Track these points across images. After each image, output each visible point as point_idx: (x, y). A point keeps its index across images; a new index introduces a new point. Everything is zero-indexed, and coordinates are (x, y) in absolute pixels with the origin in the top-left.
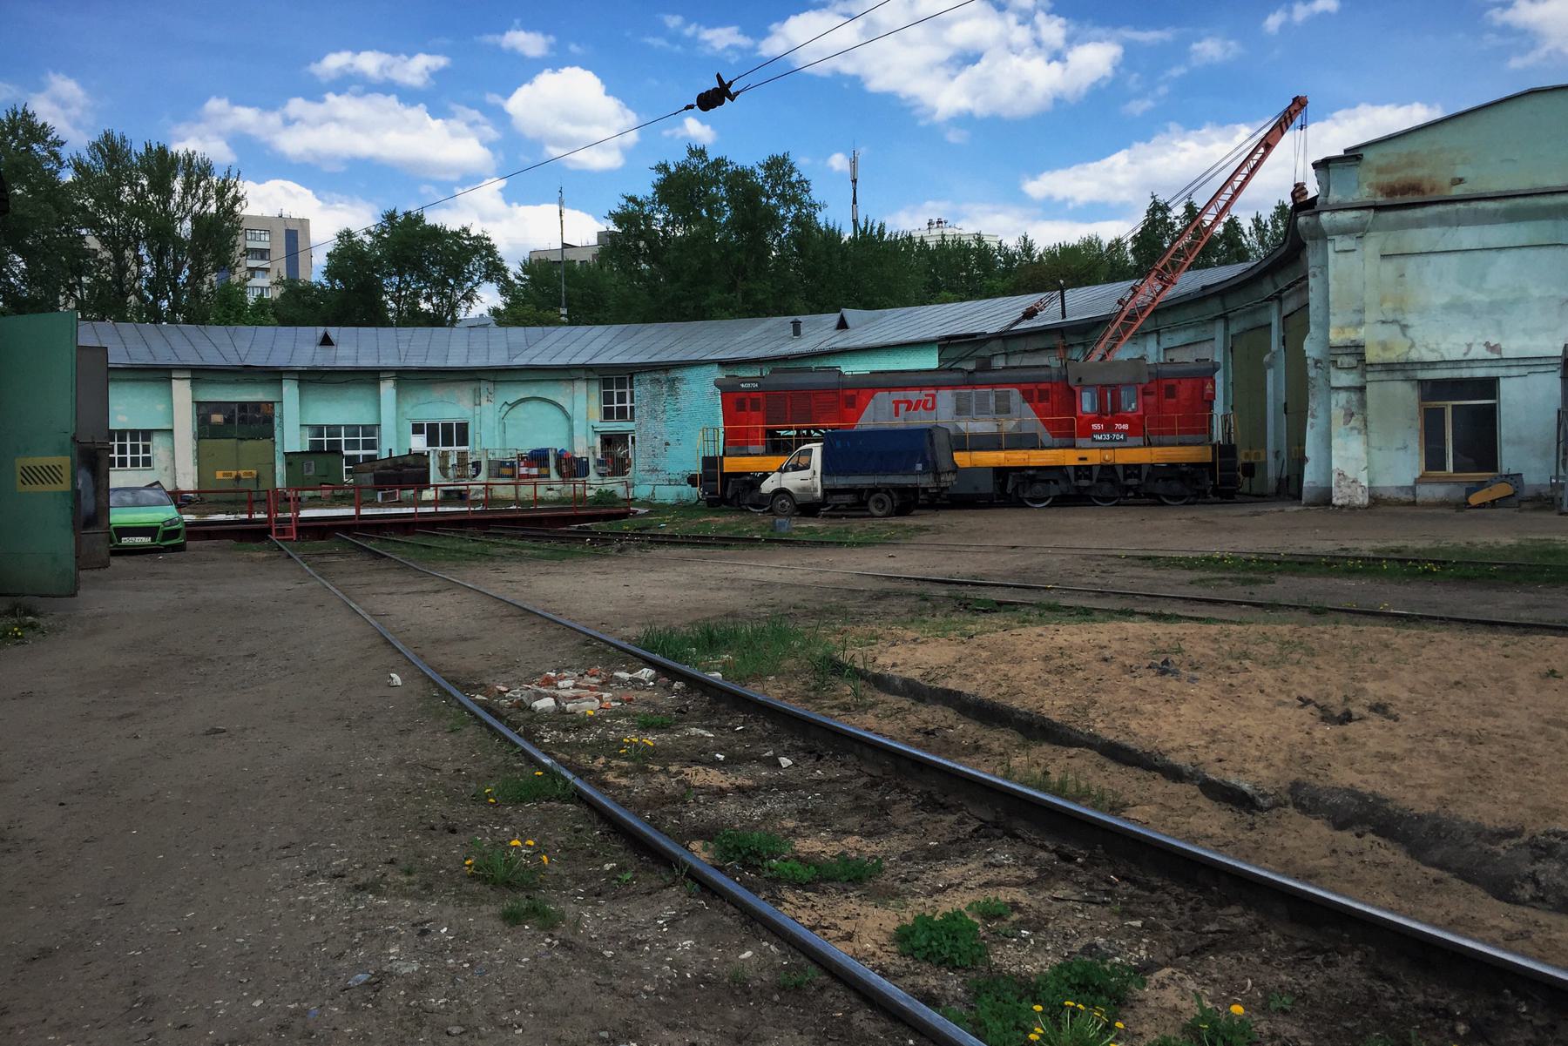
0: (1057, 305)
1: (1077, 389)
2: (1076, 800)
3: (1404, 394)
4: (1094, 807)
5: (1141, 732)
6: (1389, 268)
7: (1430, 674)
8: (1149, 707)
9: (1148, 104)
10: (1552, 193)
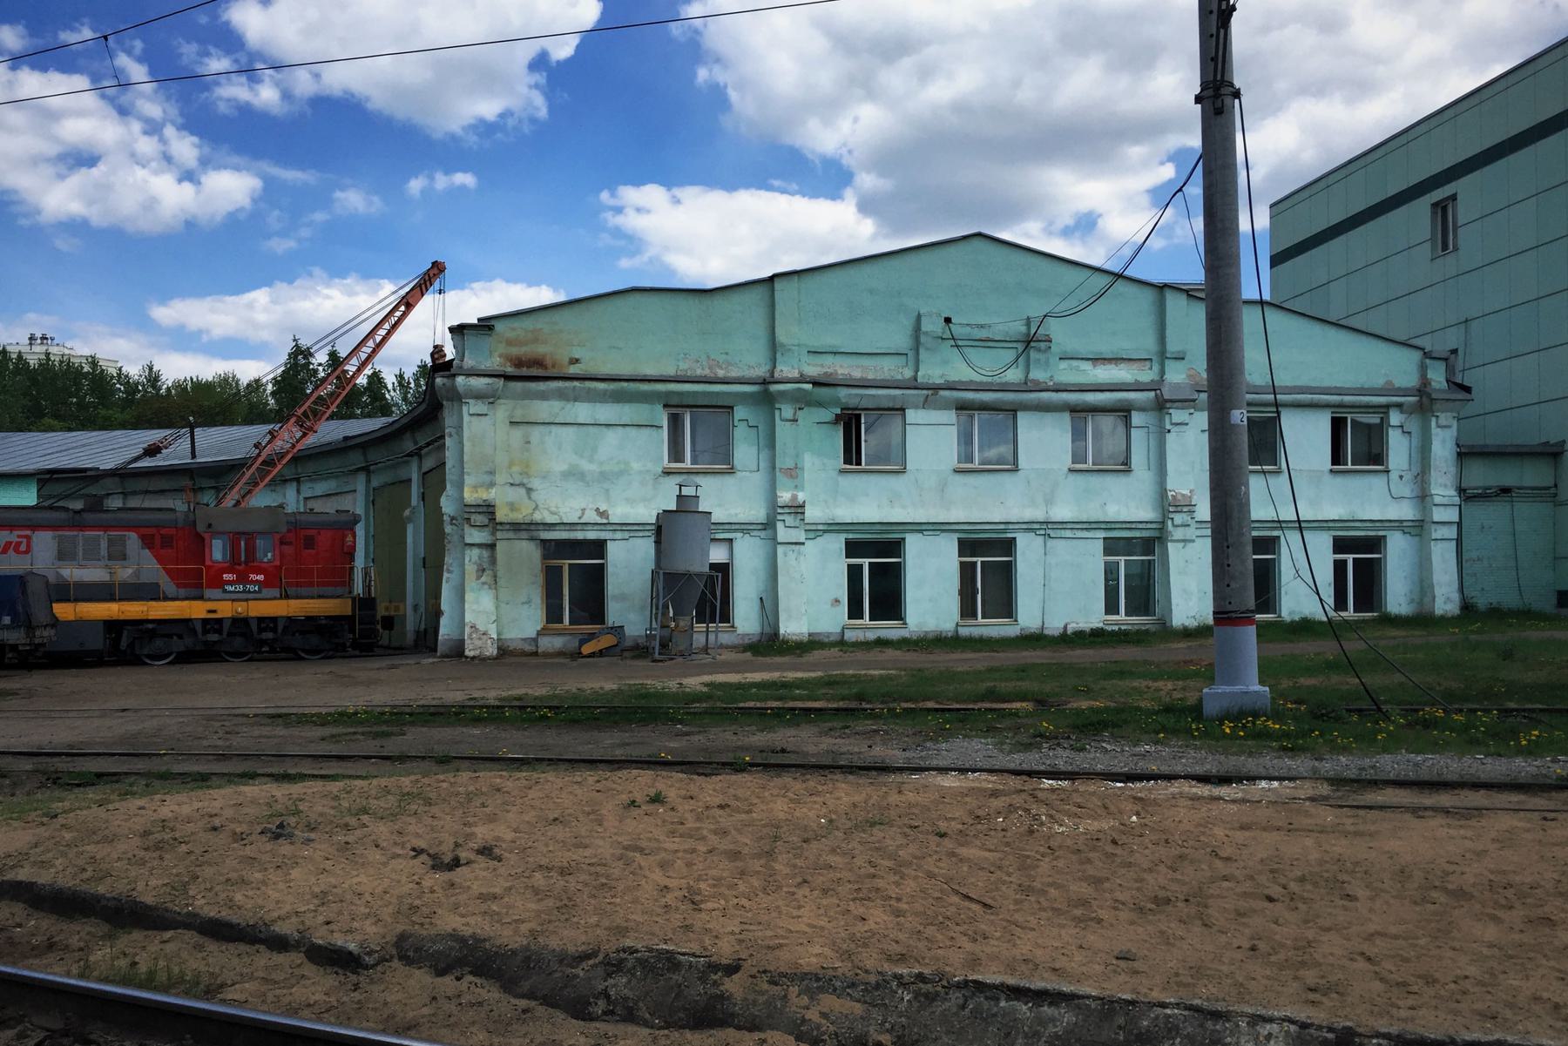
0: (187, 444)
1: (206, 536)
2: (165, 989)
3: (529, 552)
4: (187, 994)
5: (245, 905)
6: (517, 433)
7: (533, 813)
8: (258, 875)
9: (291, 244)
10: (650, 381)
